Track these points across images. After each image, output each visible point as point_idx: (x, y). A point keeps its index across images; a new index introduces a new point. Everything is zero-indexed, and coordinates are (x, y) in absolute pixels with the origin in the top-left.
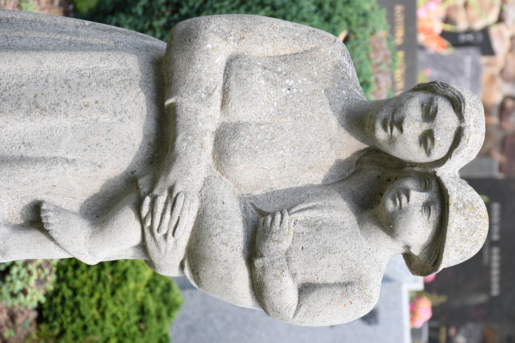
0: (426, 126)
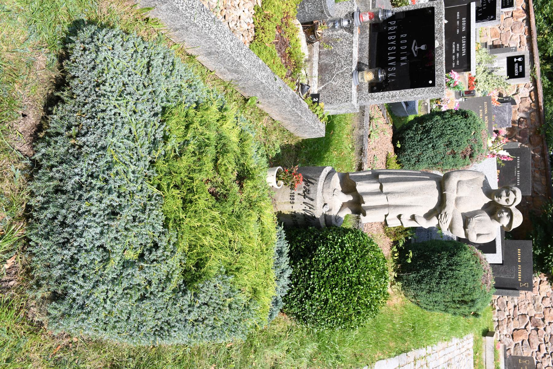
0: (507, 198)
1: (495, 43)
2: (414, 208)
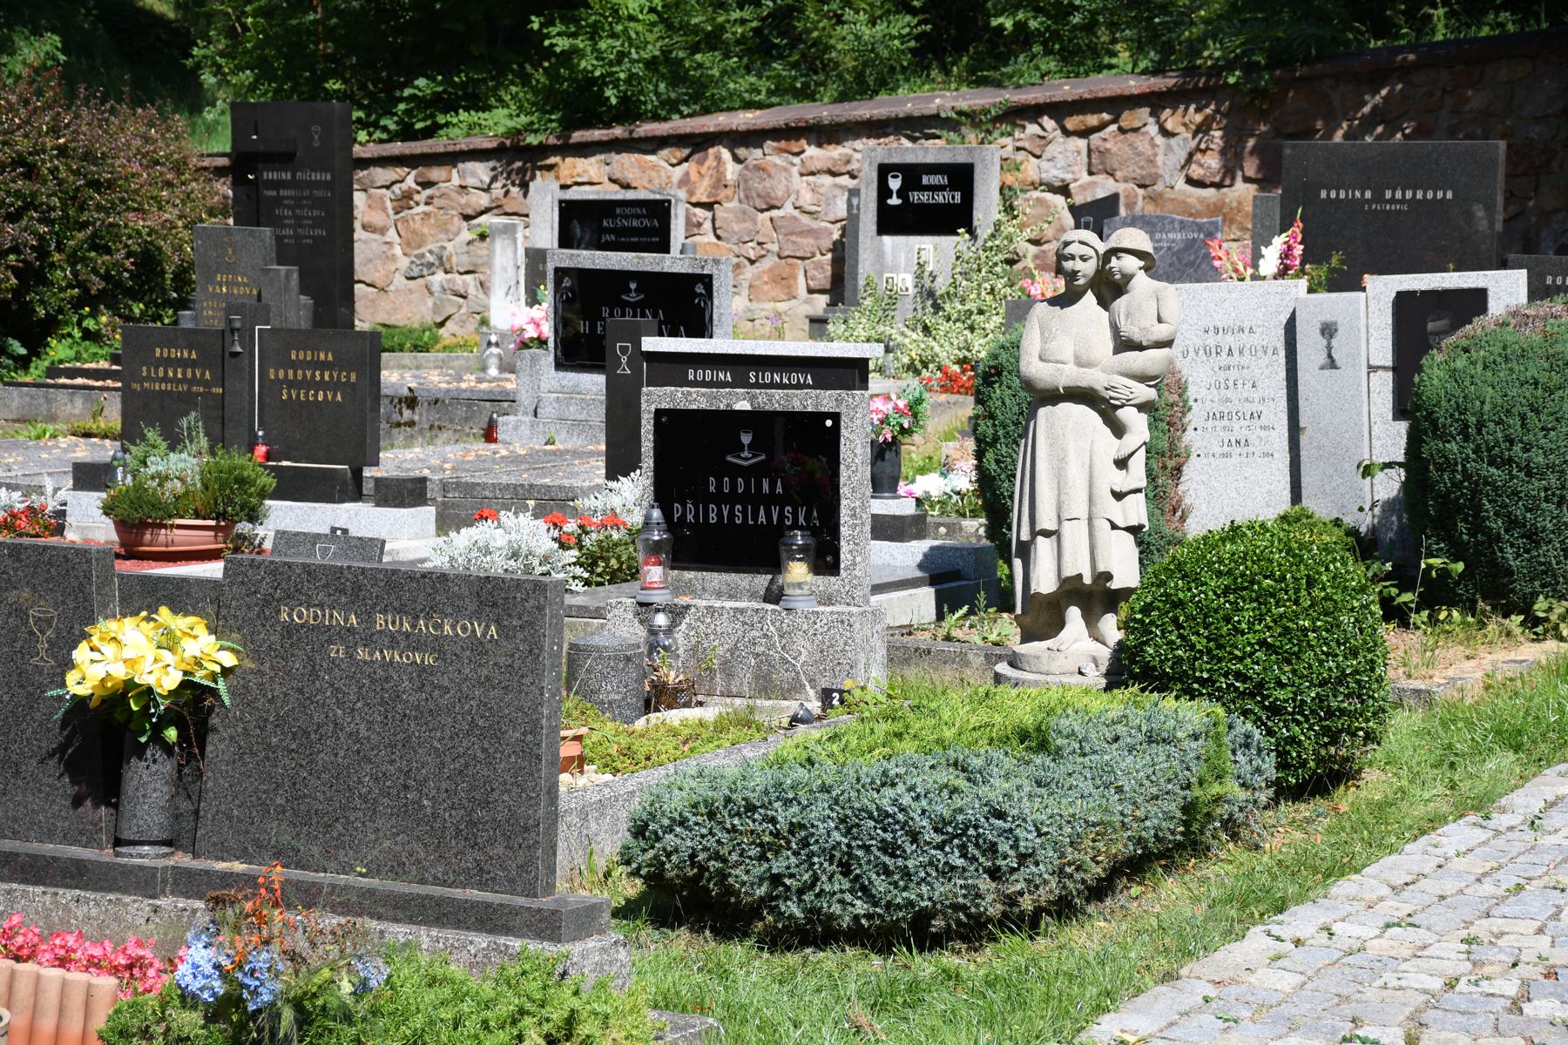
0: (1078, 259)
1: (823, 277)
2: (1094, 458)
